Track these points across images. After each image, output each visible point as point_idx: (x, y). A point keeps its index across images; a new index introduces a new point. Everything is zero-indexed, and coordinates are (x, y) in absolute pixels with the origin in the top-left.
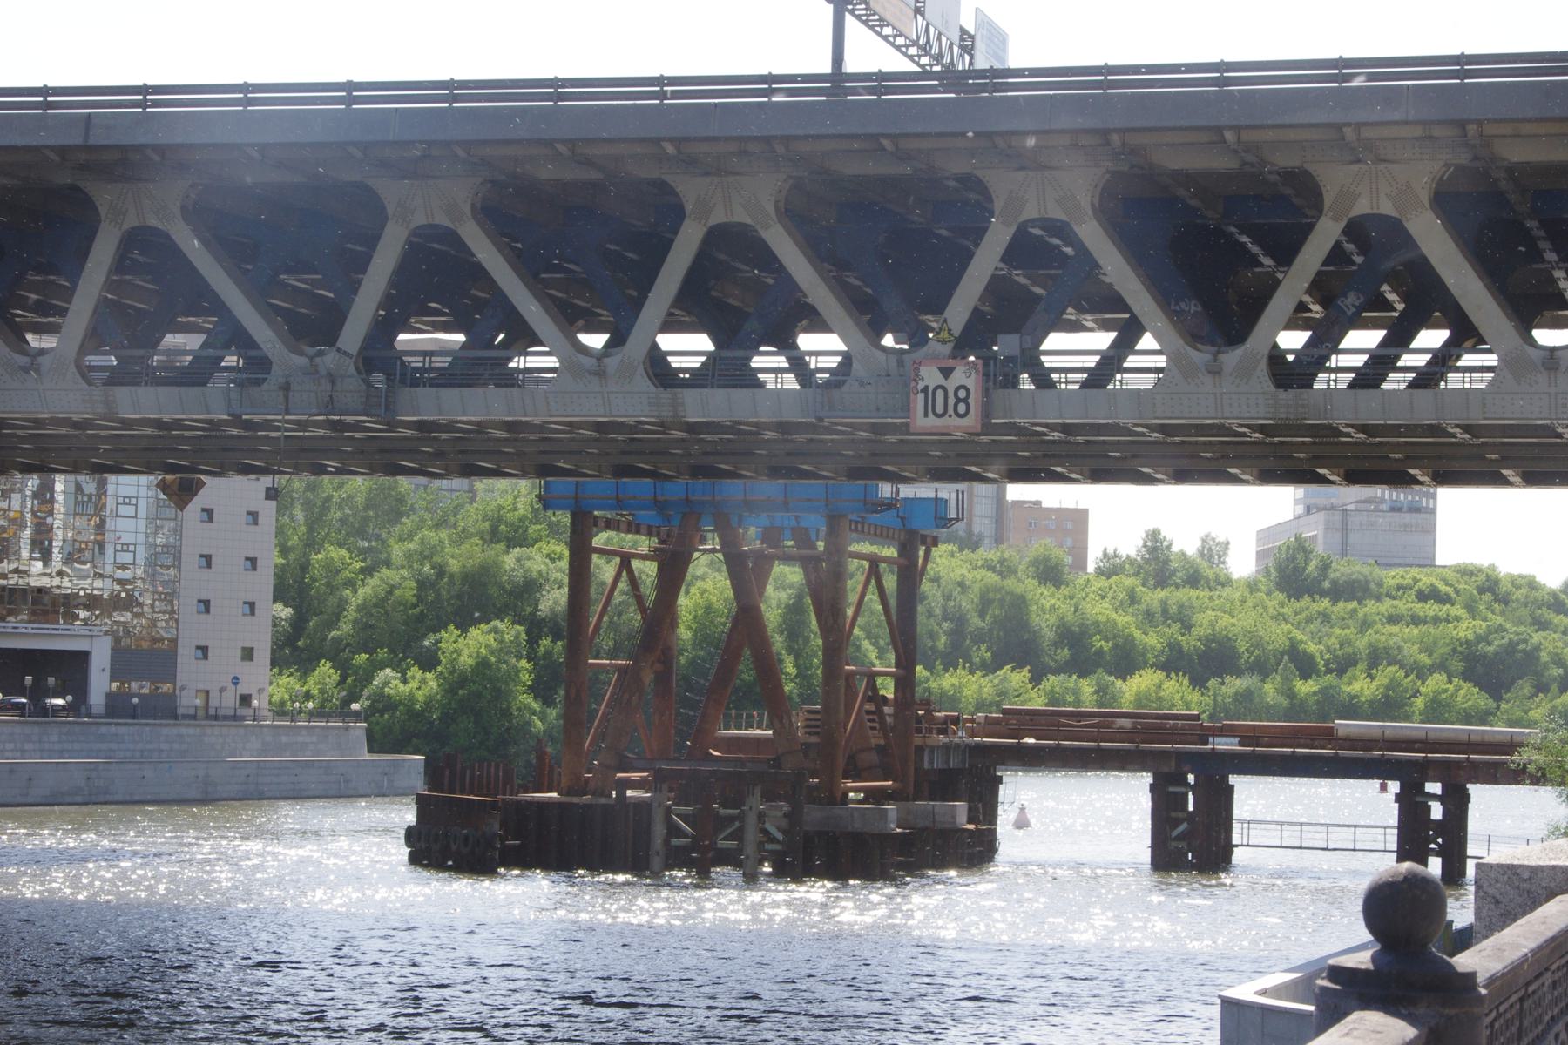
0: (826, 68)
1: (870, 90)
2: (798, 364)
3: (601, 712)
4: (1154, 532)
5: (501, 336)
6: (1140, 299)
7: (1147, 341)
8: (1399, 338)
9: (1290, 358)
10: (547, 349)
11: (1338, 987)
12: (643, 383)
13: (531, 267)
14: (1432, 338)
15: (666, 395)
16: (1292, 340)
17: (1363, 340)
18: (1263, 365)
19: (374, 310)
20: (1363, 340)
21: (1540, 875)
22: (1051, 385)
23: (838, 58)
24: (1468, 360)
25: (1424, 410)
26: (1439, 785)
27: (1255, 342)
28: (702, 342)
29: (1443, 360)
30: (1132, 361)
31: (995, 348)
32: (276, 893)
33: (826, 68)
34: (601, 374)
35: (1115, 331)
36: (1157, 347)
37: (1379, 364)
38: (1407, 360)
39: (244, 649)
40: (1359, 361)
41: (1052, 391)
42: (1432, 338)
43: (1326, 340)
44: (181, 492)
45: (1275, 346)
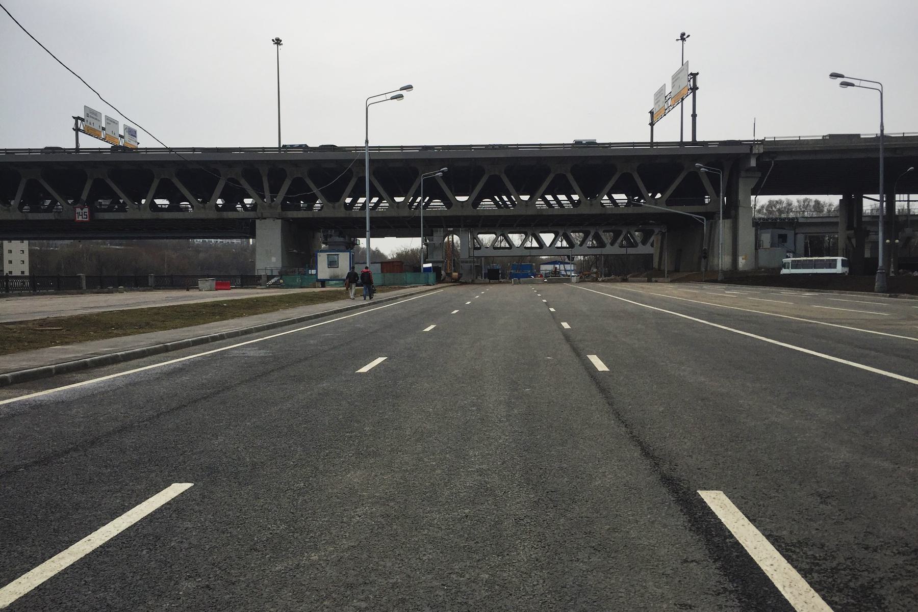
0: (680, 141)
1: (144, 152)
2: (244, 205)
9: (576, 201)
10: (440, 201)
12: (343, 209)
13: (576, 179)
14: (375, 200)
16: (348, 200)
17: (362, 200)
18: (343, 206)
19: (19, 200)
22: (564, 207)
23: (882, 131)
26: (28, 275)
27: (341, 201)
28: (623, 196)
29: (377, 204)
30: (381, 205)
32: (300, 501)
33: (680, 141)
35: (528, 195)
36: (567, 199)
40: (361, 205)
41: (508, 209)
42: (375, 200)
43: (354, 201)
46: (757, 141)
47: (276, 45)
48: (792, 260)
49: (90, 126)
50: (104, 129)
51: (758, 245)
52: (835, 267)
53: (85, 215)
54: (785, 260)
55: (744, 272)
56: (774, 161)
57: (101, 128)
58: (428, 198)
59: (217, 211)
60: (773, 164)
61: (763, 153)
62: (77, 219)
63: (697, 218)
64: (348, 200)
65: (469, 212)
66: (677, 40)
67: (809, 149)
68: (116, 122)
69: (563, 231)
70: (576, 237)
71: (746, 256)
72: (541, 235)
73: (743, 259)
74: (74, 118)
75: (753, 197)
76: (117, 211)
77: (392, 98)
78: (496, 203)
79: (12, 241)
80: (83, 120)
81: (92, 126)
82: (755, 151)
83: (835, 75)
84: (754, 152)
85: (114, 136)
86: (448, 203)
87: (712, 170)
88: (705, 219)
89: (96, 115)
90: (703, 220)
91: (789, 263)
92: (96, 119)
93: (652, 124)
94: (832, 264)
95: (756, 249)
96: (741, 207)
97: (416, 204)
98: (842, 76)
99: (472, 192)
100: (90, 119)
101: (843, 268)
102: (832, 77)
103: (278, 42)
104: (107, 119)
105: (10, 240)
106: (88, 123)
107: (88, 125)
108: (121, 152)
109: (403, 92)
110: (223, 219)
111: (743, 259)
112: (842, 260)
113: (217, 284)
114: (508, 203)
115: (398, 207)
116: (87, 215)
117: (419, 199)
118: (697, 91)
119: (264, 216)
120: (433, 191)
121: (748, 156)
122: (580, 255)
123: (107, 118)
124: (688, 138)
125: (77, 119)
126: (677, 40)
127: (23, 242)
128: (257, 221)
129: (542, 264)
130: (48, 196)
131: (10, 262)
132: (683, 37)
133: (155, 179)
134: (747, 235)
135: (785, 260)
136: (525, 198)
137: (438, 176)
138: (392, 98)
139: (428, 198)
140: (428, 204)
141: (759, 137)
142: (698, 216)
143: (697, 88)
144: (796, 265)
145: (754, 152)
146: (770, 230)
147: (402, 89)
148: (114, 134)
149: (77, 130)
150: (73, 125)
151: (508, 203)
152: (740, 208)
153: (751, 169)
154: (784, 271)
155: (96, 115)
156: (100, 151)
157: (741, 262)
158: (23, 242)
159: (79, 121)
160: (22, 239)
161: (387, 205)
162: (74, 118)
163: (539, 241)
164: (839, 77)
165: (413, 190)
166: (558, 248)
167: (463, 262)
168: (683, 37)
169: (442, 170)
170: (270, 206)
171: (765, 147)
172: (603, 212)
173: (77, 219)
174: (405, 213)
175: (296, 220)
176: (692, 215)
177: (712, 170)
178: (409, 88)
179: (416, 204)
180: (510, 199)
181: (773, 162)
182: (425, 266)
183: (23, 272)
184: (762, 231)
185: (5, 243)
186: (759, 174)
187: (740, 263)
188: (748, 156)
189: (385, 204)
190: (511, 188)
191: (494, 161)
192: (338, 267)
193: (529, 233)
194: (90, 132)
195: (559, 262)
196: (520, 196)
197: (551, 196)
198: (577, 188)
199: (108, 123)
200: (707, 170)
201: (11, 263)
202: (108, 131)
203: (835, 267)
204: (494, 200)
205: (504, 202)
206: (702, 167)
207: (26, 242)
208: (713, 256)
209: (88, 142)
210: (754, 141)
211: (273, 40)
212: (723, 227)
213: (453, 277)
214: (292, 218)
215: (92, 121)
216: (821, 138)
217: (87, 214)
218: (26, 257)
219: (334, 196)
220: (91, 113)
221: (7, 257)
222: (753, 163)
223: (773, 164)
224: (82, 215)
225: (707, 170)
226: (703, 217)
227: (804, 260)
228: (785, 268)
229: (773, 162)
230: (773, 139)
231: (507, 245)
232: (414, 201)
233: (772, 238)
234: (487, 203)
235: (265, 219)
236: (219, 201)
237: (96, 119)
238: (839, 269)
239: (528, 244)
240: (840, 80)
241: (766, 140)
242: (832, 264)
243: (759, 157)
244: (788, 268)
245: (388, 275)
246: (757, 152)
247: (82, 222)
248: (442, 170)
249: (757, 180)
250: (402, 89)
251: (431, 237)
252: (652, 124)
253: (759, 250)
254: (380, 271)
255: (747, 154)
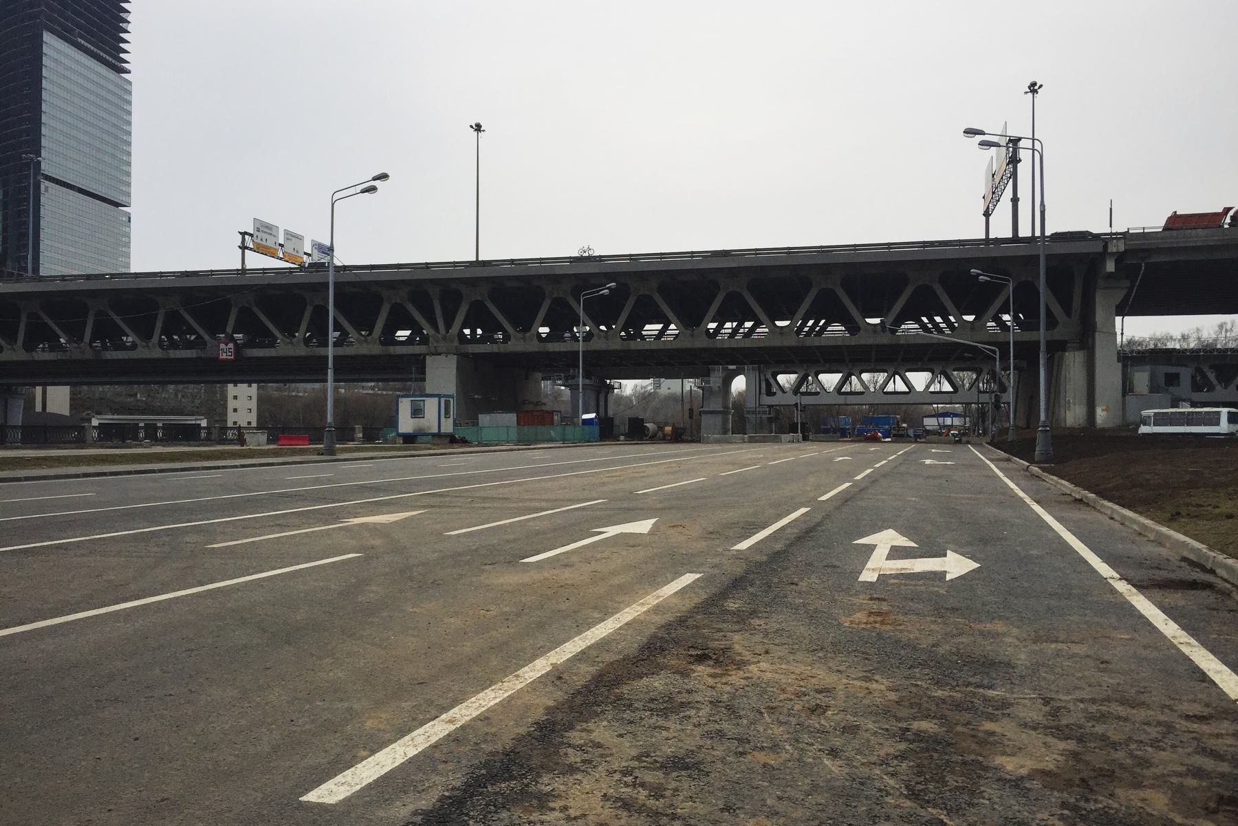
0: (1009, 235)
1: (921, 247)
3: (1012, 358)
4: (1182, 336)
5: (1021, 315)
6: (671, 315)
7: (672, 326)
8: (740, 325)
11: (915, 545)
12: (535, 341)
14: (748, 324)
15: (542, 344)
16: (712, 325)
20: (811, 323)
21: (399, 736)
24: (758, 330)
25: (748, 344)
29: (752, 330)
31: (614, 327)
33: (474, 259)
34: (366, 341)
37: (735, 331)
38: (741, 331)
39: (234, 396)
43: (721, 326)
44: (447, 356)
45: (538, 332)
46: (1116, 234)
47: (476, 133)
48: (1155, 413)
49: (261, 242)
50: (281, 245)
51: (1127, 388)
52: (1218, 424)
53: (229, 352)
54: (1145, 413)
55: (1103, 430)
56: (1145, 263)
57: (277, 245)
58: (823, 321)
59: (381, 345)
60: (1143, 268)
61: (1123, 252)
62: (221, 357)
63: (987, 349)
64: (712, 325)
65: (885, 339)
66: (1026, 93)
67: (1199, 244)
68: (300, 237)
69: (1196, 365)
70: (967, 377)
71: (1108, 407)
72: (907, 374)
73: (1103, 410)
74: (240, 233)
75: (1118, 319)
76: (420, 343)
77: (363, 191)
78: (923, 326)
79: (238, 385)
80: (251, 235)
81: (264, 243)
82: (1112, 248)
83: (970, 132)
84: (1109, 251)
85: (297, 254)
86: (853, 327)
87: (997, 278)
88: (997, 349)
89: (270, 229)
90: (994, 352)
91: (1149, 417)
92: (271, 234)
93: (987, 214)
94: (1214, 420)
95: (1124, 394)
96: (1098, 331)
97: (806, 329)
98: (982, 133)
99: (889, 310)
100: (260, 234)
101: (1231, 425)
102: (966, 135)
103: (478, 128)
104: (287, 234)
105: (235, 383)
106: (259, 239)
107: (259, 241)
108: (107, 275)
109: (377, 183)
110: (391, 356)
111: (1103, 410)
112: (1229, 413)
113: (268, 439)
114: (930, 326)
115: (875, 332)
116: (231, 352)
117: (811, 323)
118: (1018, 165)
119: (439, 351)
120: (829, 309)
121: (1104, 254)
122: (866, 405)
123: (287, 233)
124: (1025, 231)
125: (243, 234)
126: (1026, 93)
127: (251, 386)
128: (428, 357)
129: (926, 417)
130: (501, 328)
131: (235, 398)
132: (1033, 88)
133: (233, 308)
134: (1109, 376)
135: (1145, 413)
136: (970, 318)
137: (603, 294)
138: (363, 191)
139: (823, 321)
140: (823, 328)
141: (1119, 227)
142: (987, 347)
143: (1020, 160)
144: (1160, 420)
145: (1109, 251)
146: (1148, 368)
147: (375, 179)
148: (297, 252)
149: (243, 247)
150: (239, 243)
151: (930, 326)
152: (1097, 333)
153: (1110, 275)
154: (1144, 429)
155: (270, 229)
156: (278, 271)
157: (1101, 415)
158: (251, 386)
159: (247, 237)
160: (250, 383)
161: (767, 330)
162: (240, 233)
163: (906, 382)
164: (978, 134)
165: (802, 311)
166: (932, 393)
167: (748, 412)
168: (1033, 88)
169: (607, 286)
170: (444, 338)
171: (1128, 243)
172: (894, 342)
173: (221, 357)
174: (791, 341)
175: (477, 357)
176: (978, 344)
177: (997, 278)
178: (383, 177)
179: (806, 329)
180: (946, 321)
181: (1143, 265)
182: (586, 416)
183: (249, 423)
184: (1135, 368)
185: (230, 386)
186: (1127, 283)
187: (1098, 417)
188: (1104, 254)
189: (763, 330)
190: (949, 305)
191: (732, 273)
192: (424, 417)
193: (937, 371)
194: (261, 249)
195: (951, 413)
196: (866, 319)
197: (939, 317)
198: (128, 331)
199: (288, 239)
200: (988, 279)
201: (234, 411)
202: (289, 248)
203: (1218, 424)
204: (920, 322)
205: (936, 325)
206: (979, 275)
207: (255, 386)
208: (1059, 406)
209: (256, 261)
210: (1111, 234)
211: (471, 127)
212: (1074, 362)
213: (666, 432)
214: (472, 354)
215: (265, 236)
216: (1161, 230)
217: (232, 350)
218: (253, 404)
219: (691, 320)
220: (265, 228)
221: (231, 404)
222: (1110, 267)
223: (1143, 268)
224: (226, 352)
225: (988, 279)
226: (994, 348)
227: (1172, 413)
228: (1145, 425)
229: (1143, 265)
230: (1142, 231)
231: (843, 390)
232: (804, 324)
233: (1153, 378)
234: (910, 326)
235: (440, 354)
236: (544, 330)
237: (271, 234)
238: (1224, 427)
239: (890, 387)
240: (979, 138)
241: (1130, 232)
242: (1214, 420)
243: (1120, 258)
244: (1150, 425)
245: (526, 428)
246: (1115, 250)
247: (225, 361)
248: (607, 286)
249: (1124, 292)
250: (375, 179)
251: (706, 379)
252: (987, 214)
253: (1127, 396)
254: (516, 425)
255: (1100, 254)
